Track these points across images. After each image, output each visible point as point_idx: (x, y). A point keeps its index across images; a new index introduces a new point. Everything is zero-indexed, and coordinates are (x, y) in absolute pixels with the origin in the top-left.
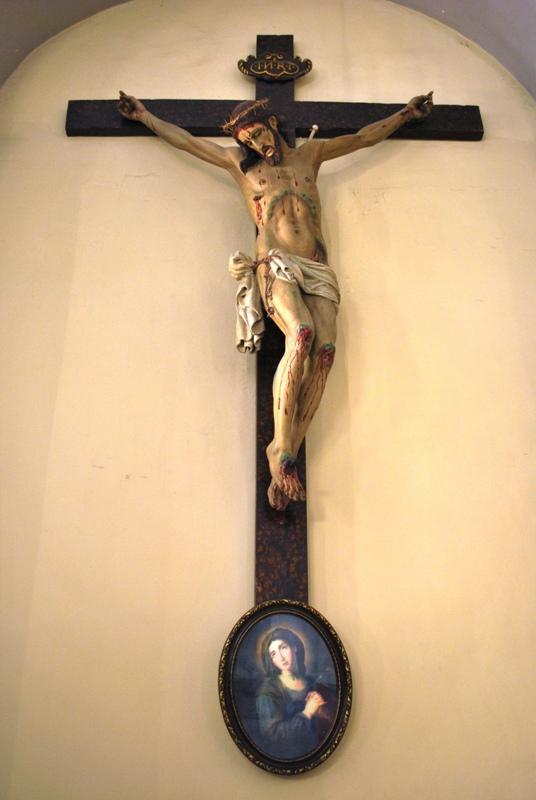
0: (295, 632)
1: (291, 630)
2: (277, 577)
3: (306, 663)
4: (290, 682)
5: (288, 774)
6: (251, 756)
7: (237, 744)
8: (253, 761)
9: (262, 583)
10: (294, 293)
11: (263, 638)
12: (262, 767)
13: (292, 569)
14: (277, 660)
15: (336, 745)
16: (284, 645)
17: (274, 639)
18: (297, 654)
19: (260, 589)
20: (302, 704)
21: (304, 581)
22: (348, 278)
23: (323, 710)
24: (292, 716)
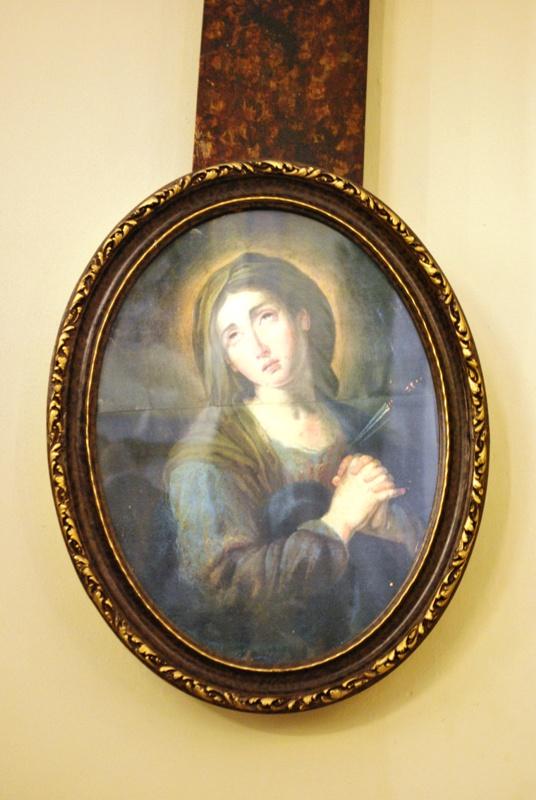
0: (304, 269)
1: (295, 262)
2: (266, 113)
3: (335, 366)
4: (288, 429)
5: (267, 710)
6: (145, 649)
7: (102, 608)
8: (153, 665)
9: (217, 132)
10: (368, 515)
11: (195, 284)
12: (178, 684)
13: (316, 92)
14: (244, 356)
15: (429, 626)
16: (269, 307)
17: (233, 287)
18: (310, 335)
19: (208, 149)
20: (319, 495)
21: (352, 130)
22: (377, 467)
23: (390, 514)
24: (289, 527)
